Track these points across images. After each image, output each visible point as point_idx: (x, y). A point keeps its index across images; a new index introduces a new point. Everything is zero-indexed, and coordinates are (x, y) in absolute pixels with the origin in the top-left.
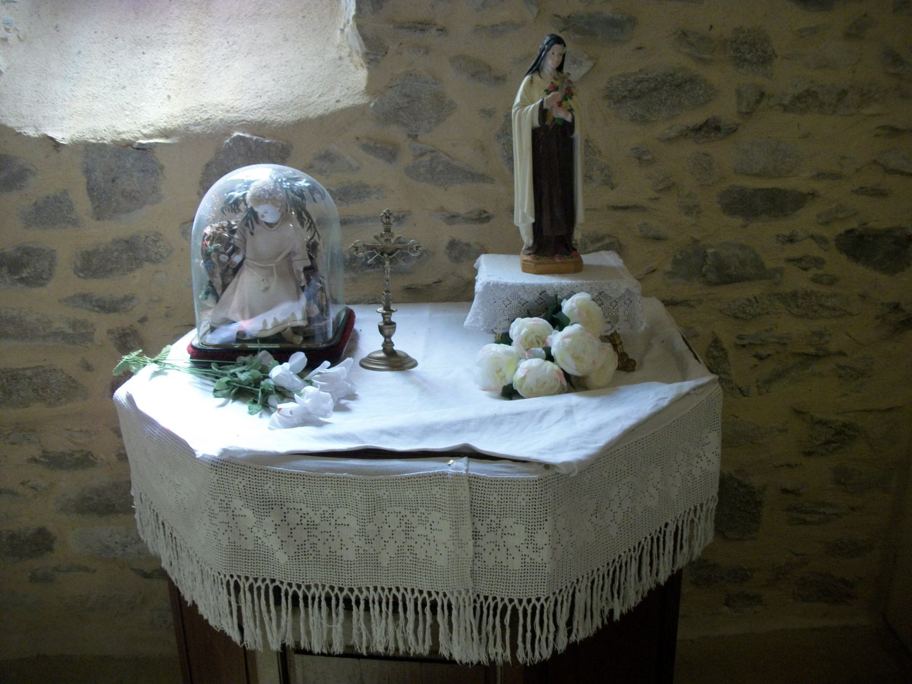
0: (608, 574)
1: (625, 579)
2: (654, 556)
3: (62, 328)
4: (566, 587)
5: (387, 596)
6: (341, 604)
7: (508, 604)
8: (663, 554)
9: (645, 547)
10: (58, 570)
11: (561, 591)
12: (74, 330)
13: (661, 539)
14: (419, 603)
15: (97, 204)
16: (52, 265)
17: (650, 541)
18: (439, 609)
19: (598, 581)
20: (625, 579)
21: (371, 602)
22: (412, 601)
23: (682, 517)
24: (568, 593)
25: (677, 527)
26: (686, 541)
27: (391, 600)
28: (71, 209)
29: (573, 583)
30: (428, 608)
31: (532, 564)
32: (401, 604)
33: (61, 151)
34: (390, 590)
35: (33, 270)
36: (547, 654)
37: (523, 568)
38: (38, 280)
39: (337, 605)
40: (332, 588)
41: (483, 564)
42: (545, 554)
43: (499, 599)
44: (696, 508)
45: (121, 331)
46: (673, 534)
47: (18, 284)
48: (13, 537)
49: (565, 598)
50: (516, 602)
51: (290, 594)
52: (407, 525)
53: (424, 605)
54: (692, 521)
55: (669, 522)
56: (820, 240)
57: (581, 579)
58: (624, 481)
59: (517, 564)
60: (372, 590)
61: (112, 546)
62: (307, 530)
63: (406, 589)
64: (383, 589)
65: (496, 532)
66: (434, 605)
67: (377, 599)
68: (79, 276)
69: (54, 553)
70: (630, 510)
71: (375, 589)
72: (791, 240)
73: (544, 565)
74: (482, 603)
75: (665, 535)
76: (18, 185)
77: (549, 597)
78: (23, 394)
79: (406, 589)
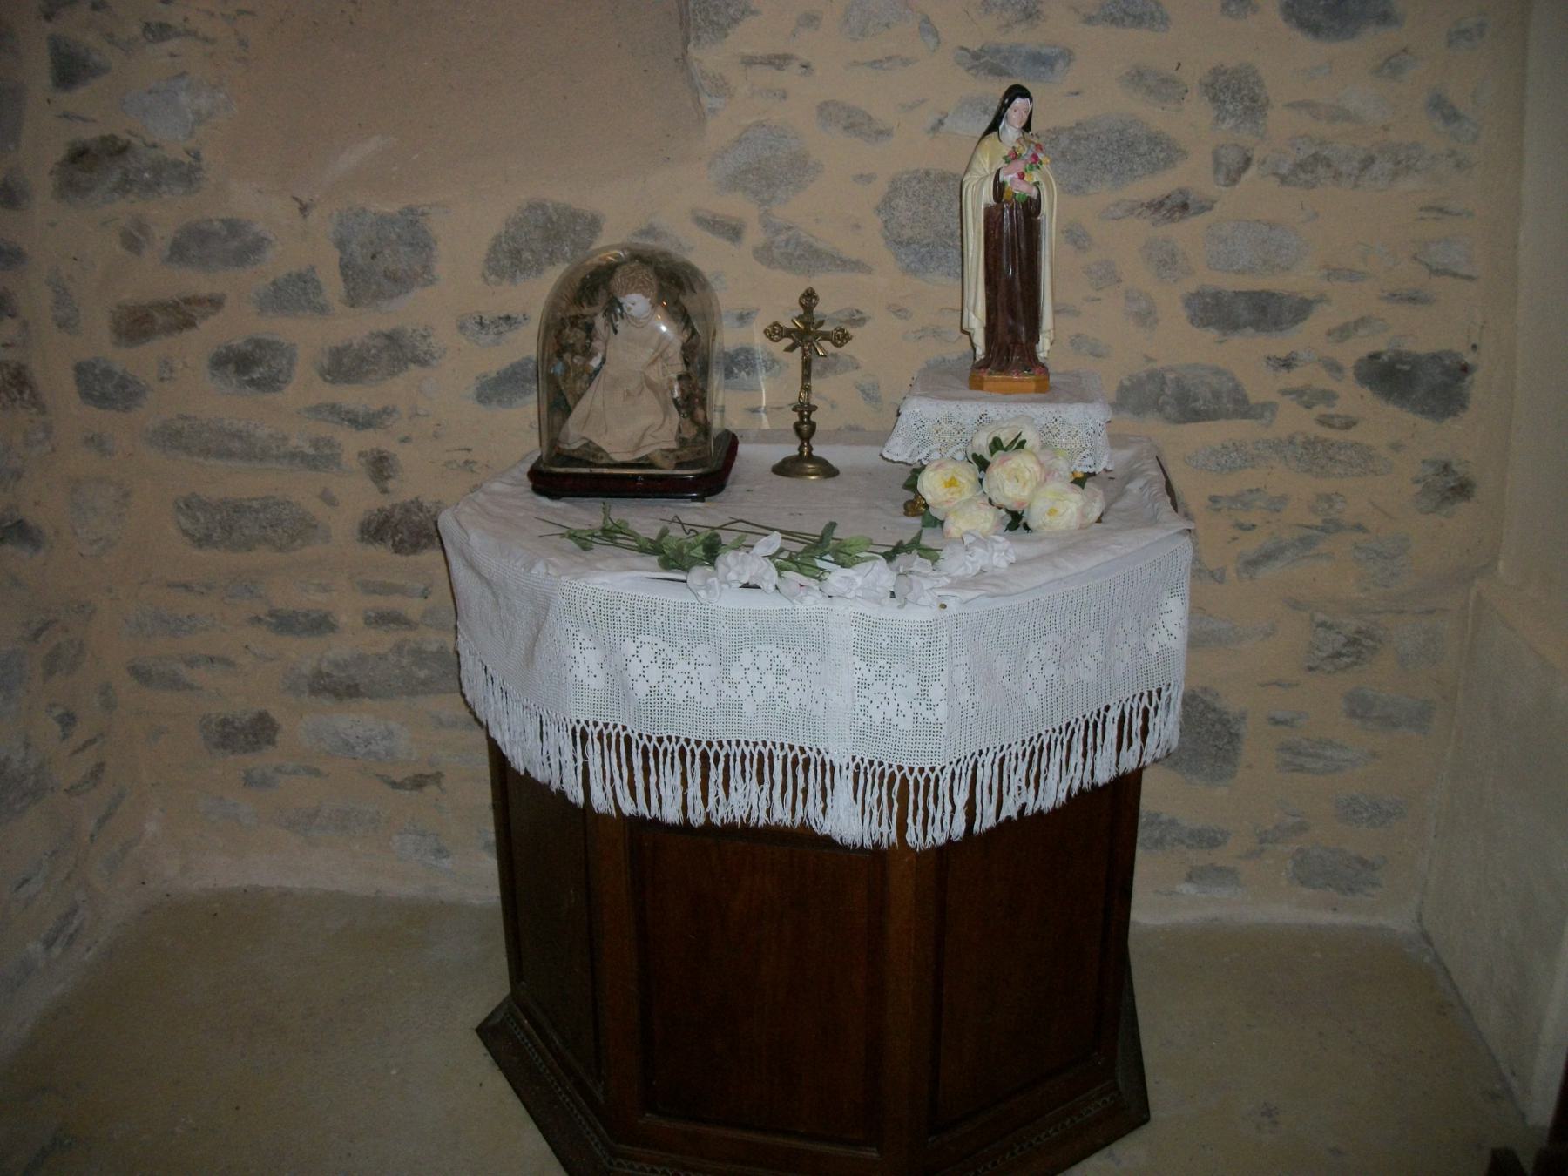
0: (1024, 755)
1: (1048, 766)
2: (1089, 747)
3: (301, 447)
4: (966, 757)
5: (751, 752)
6: (697, 761)
7: (897, 772)
8: (1102, 746)
9: (1076, 730)
10: (280, 771)
11: (959, 761)
12: (317, 449)
13: (1100, 725)
14: (789, 760)
15: (351, 285)
16: (291, 363)
17: (1083, 724)
18: (812, 767)
19: (1010, 760)
20: (1048, 766)
21: (731, 758)
22: (781, 757)
23: (1129, 702)
24: (968, 765)
25: (1123, 712)
26: (1136, 735)
27: (756, 757)
28: (318, 289)
29: (974, 754)
30: (800, 767)
31: (925, 725)
32: (766, 760)
33: (308, 215)
34: (755, 744)
35: (267, 369)
36: (941, 841)
37: (915, 729)
38: (271, 383)
39: (693, 763)
40: (688, 741)
41: (869, 719)
42: (942, 711)
43: (886, 765)
44: (1150, 693)
45: (375, 453)
46: (1116, 721)
47: (248, 387)
48: (225, 722)
49: (964, 771)
50: (906, 770)
51: (641, 746)
52: (779, 668)
53: (795, 763)
54: (1146, 711)
55: (1111, 705)
56: (1334, 368)
57: (985, 751)
58: (1044, 639)
59: (905, 725)
60: (734, 743)
61: (352, 741)
62: (662, 670)
63: (774, 744)
64: (747, 743)
65: (885, 681)
66: (807, 761)
67: (739, 753)
68: (325, 380)
69: (276, 747)
70: (1055, 680)
71: (738, 742)
72: (1287, 364)
73: (939, 726)
74: (866, 768)
75: (1104, 721)
76: (252, 258)
77: (945, 767)
78: (247, 532)
79: (774, 744)
